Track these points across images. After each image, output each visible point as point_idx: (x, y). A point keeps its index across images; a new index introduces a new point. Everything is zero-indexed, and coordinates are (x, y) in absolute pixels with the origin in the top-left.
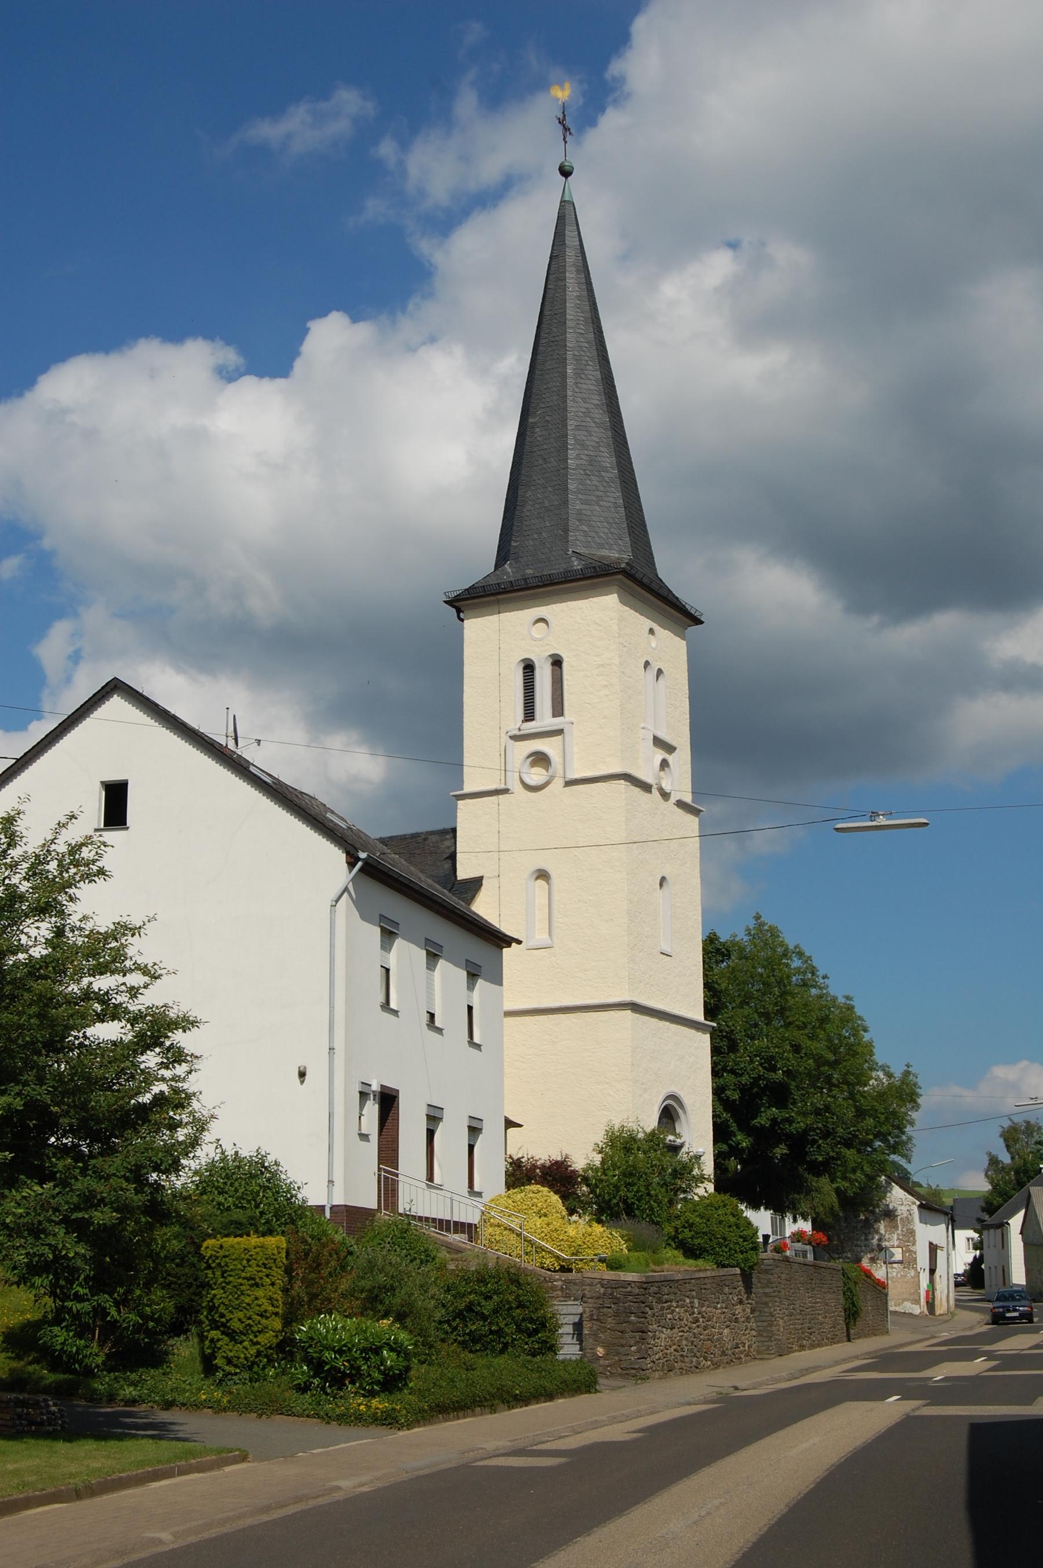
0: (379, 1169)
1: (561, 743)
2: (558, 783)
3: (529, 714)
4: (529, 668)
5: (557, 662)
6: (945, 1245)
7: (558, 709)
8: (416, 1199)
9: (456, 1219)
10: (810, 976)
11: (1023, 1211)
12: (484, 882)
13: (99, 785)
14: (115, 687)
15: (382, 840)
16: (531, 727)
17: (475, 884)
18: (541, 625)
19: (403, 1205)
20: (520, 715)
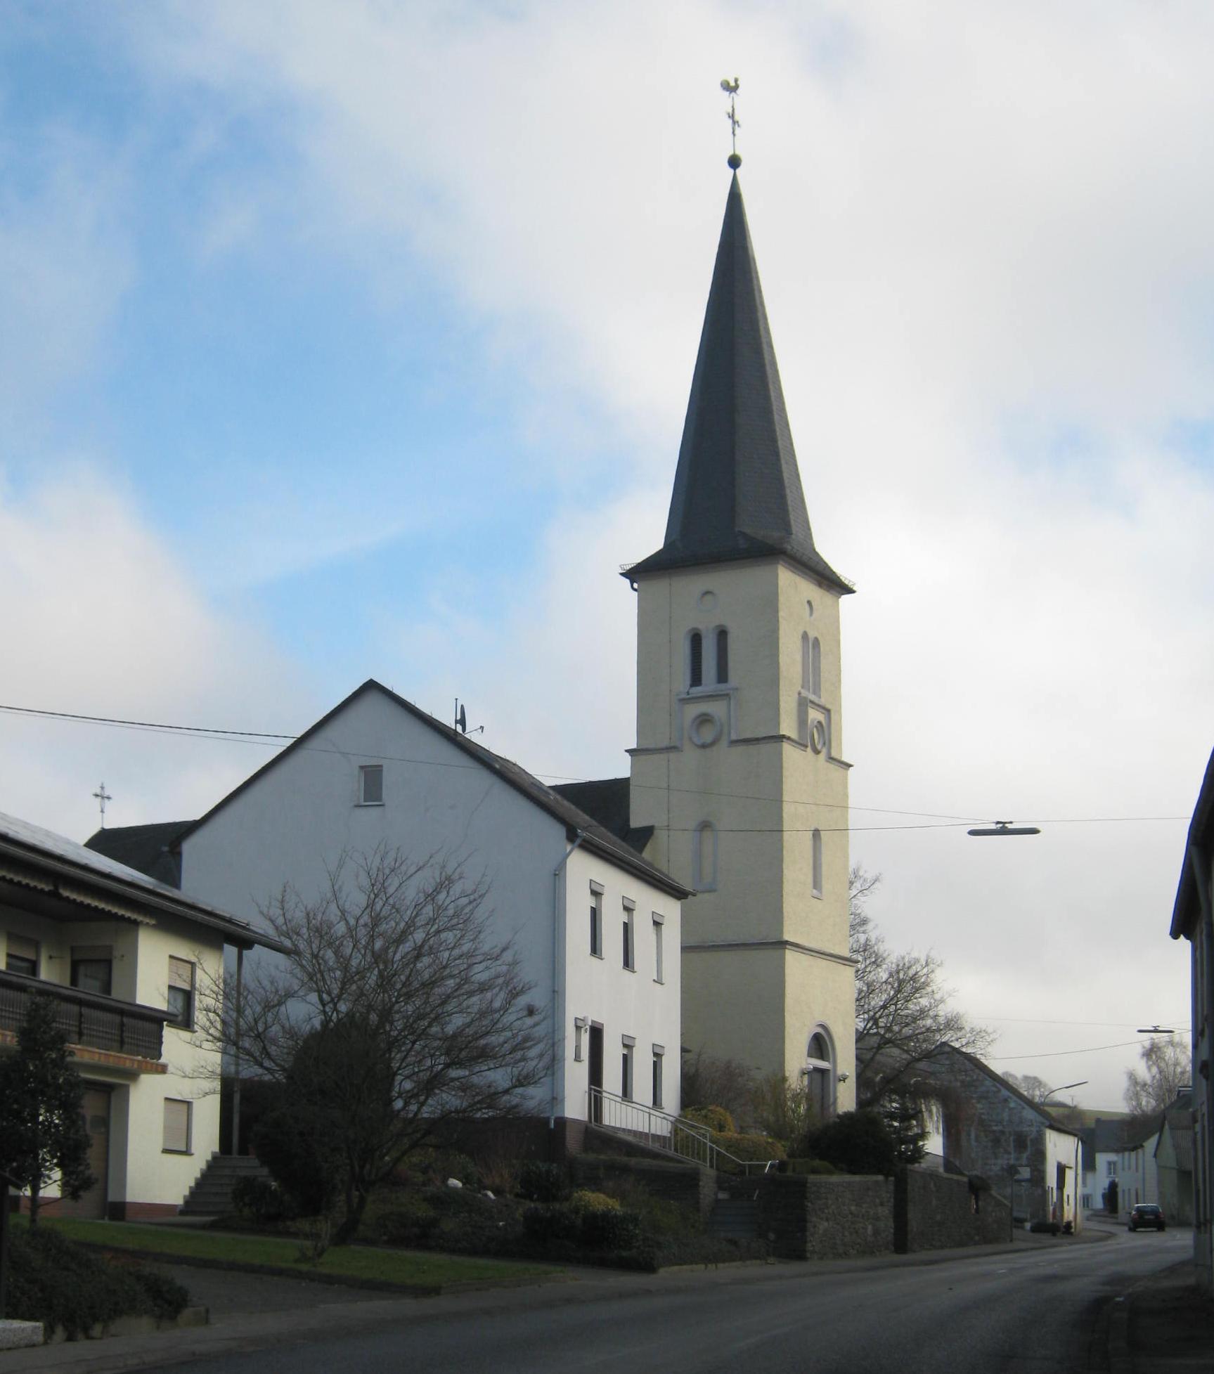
0: (590, 1089)
1: (804, 959)
2: (724, 743)
3: (696, 679)
4: (696, 640)
5: (722, 634)
6: (1073, 1165)
7: (722, 676)
8: (616, 1116)
9: (653, 1131)
10: (196, 1179)
11: (1156, 1137)
12: (656, 832)
13: (356, 771)
14: (371, 686)
15: (554, 788)
16: (697, 691)
17: (646, 833)
18: (708, 597)
19: (607, 1120)
20: (688, 682)
